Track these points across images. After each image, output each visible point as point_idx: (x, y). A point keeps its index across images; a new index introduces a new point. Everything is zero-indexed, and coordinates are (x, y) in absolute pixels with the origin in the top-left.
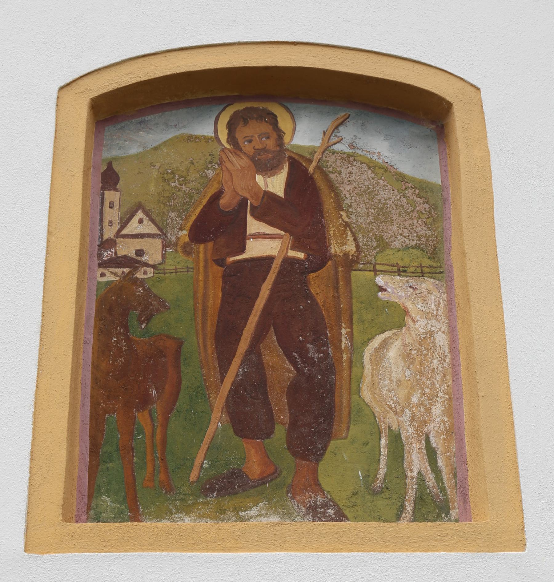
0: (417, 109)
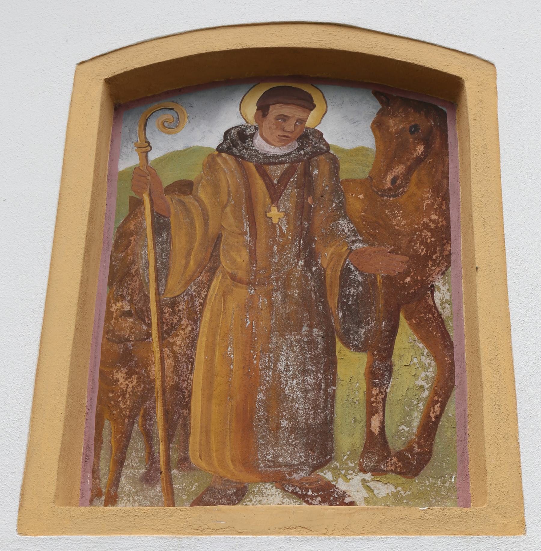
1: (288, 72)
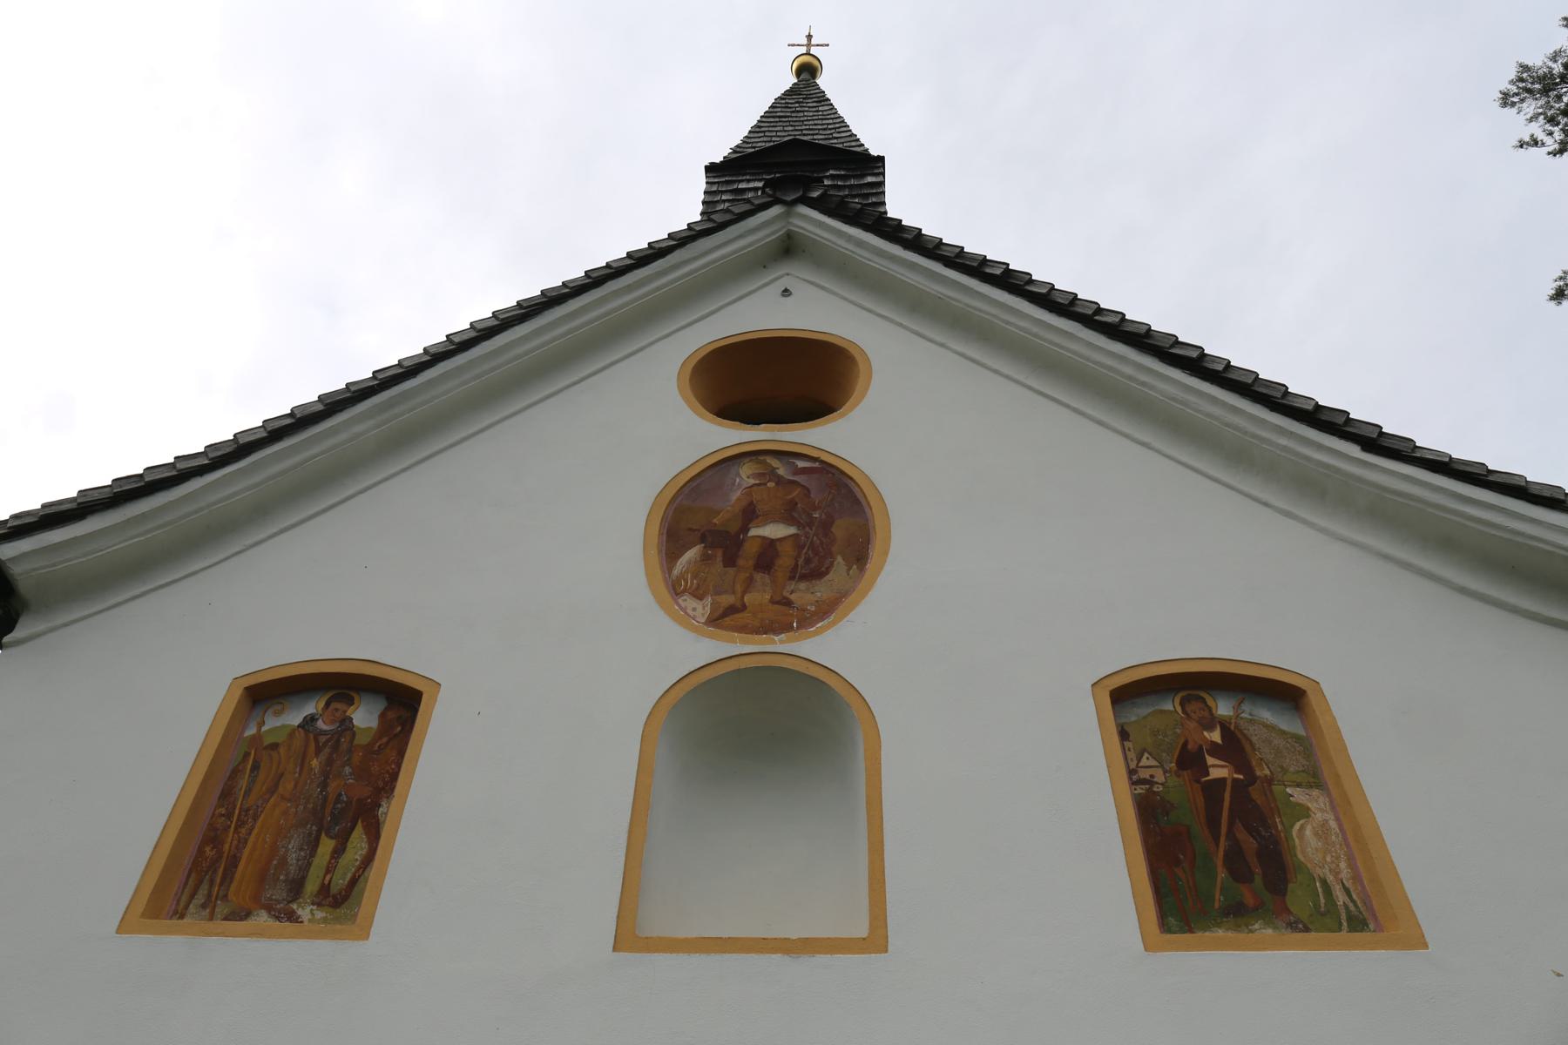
0: (1287, 694)
1: (342, 685)
